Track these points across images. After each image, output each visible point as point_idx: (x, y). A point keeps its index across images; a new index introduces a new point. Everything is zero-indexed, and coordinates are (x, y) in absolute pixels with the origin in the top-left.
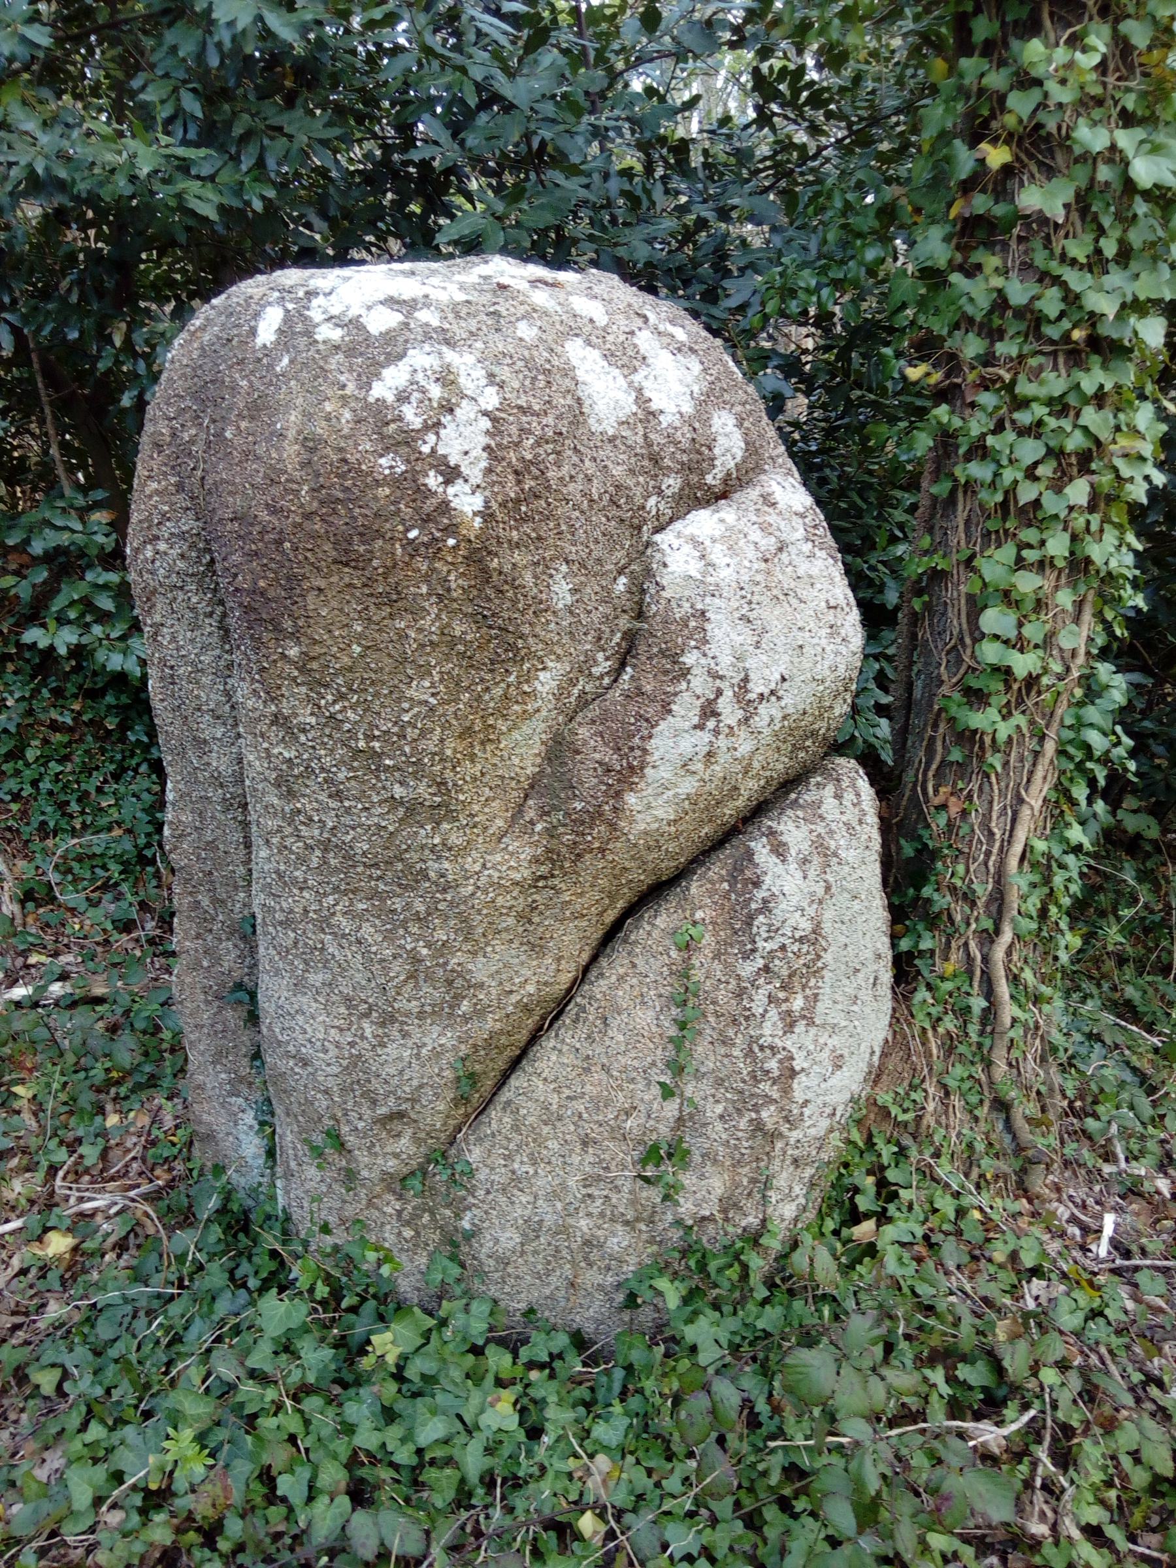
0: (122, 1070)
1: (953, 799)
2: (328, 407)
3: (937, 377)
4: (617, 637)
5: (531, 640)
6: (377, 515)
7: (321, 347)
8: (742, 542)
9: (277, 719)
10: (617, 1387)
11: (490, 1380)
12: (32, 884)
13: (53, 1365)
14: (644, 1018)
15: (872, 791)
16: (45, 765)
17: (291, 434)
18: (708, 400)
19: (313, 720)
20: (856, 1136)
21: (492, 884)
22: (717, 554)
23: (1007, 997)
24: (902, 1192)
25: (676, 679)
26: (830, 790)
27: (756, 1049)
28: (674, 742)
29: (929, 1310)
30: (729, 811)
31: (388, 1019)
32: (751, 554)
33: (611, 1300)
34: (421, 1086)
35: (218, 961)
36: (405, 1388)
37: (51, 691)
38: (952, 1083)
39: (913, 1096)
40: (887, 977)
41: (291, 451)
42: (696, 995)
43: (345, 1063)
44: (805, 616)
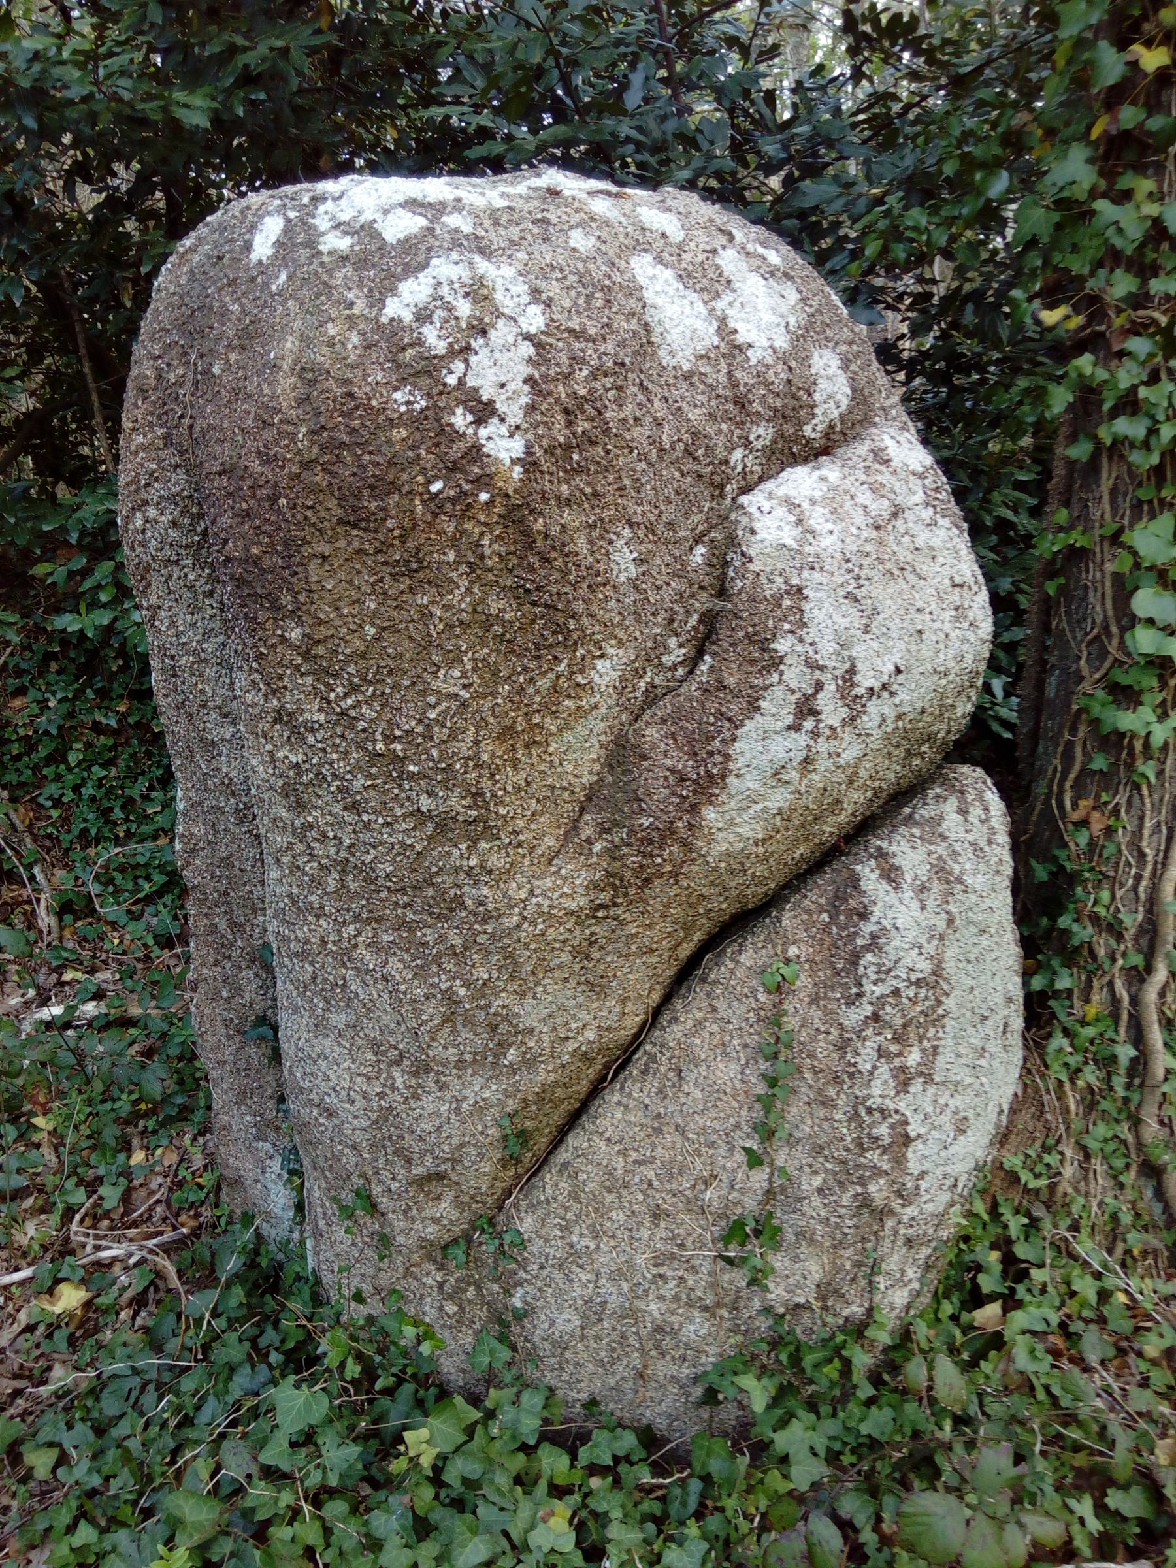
0: (152, 1101)
1: (1096, 815)
2: (331, 330)
3: (1078, 321)
4: (694, 619)
6: (391, 463)
7: (326, 259)
8: (848, 505)
9: (280, 716)
10: (692, 1505)
11: (543, 1486)
12: (70, 895)
13: (51, 1445)
14: (727, 1072)
15: (1001, 805)
17: (286, 365)
18: (807, 335)
19: (322, 718)
22: (818, 519)
23: (1159, 1045)
25: (765, 670)
26: (952, 804)
27: (863, 1113)
28: (763, 746)
29: (1070, 1419)
30: (829, 829)
31: (421, 1068)
32: (859, 518)
33: (688, 1394)
34: (462, 1145)
35: (237, 991)
36: (443, 1493)
37: (96, 692)
38: (1093, 1145)
41: (286, 384)
42: (789, 1047)
43: (374, 1116)
44: (924, 595)
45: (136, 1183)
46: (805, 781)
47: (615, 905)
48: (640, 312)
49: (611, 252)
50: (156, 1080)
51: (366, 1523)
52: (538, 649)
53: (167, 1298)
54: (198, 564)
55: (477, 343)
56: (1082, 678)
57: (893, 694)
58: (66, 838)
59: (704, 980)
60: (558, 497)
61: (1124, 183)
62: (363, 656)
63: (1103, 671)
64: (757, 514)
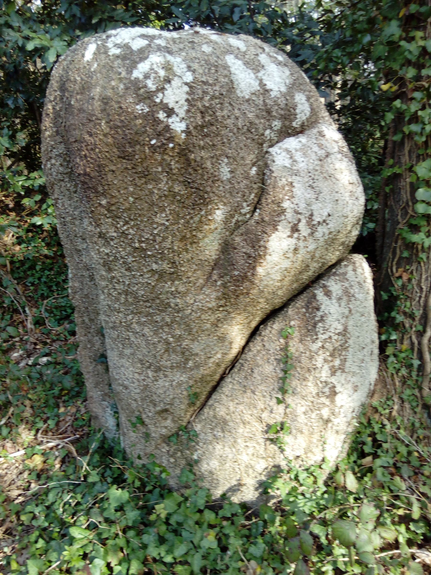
1: (405, 274)
3: (395, 88)
5: (211, 195)
6: (136, 133)
7: (111, 58)
8: (309, 152)
9: (101, 235)
11: (205, 526)
16: (43, 272)
17: (96, 98)
18: (294, 87)
19: (115, 234)
21: (199, 309)
22: (298, 156)
25: (279, 215)
26: (350, 268)
27: (319, 382)
29: (397, 497)
30: (306, 277)
31: (158, 369)
32: (314, 157)
34: (174, 398)
35: (93, 345)
36: (170, 527)
38: (405, 397)
39: (388, 403)
40: (376, 351)
41: (97, 104)
43: (141, 388)
45: (61, 419)
47: (226, 306)
48: (229, 75)
49: (218, 53)
50: (68, 382)
51: (141, 539)
54: (71, 180)
55: (167, 86)
57: (327, 224)
60: (199, 146)
61: (411, 34)
63: (406, 220)
64: (275, 155)
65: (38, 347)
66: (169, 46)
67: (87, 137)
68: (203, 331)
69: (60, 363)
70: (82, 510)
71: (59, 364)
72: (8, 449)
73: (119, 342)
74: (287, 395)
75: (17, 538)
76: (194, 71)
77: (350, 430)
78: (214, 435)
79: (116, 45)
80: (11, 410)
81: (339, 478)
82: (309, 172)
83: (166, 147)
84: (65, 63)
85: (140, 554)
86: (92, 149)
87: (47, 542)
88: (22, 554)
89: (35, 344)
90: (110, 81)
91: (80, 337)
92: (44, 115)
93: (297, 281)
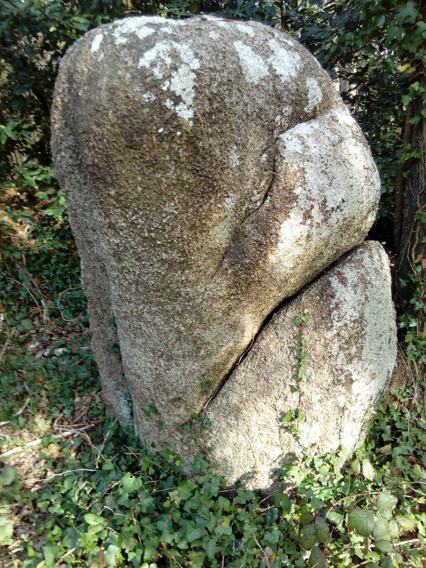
3: (413, 70)
6: (144, 122)
7: (118, 47)
8: (322, 137)
9: (111, 226)
16: (58, 265)
18: (305, 71)
19: (124, 225)
20: (382, 409)
22: (310, 142)
24: (403, 433)
25: (290, 202)
26: (367, 254)
27: (334, 370)
29: (417, 486)
30: (319, 264)
31: (170, 358)
32: (326, 142)
34: (187, 387)
35: (106, 335)
40: (395, 339)
41: (104, 94)
43: (154, 377)
45: (77, 408)
46: (308, 245)
47: (237, 294)
49: (226, 40)
50: (83, 373)
51: (155, 526)
52: (203, 194)
53: (87, 448)
54: (81, 172)
55: (174, 74)
56: (418, 208)
57: (341, 210)
58: (51, 289)
59: (273, 323)
60: (207, 133)
62: (138, 199)
64: (286, 141)
65: (54, 338)
66: (175, 33)
67: (94, 128)
68: (215, 320)
69: (75, 354)
70: (97, 498)
71: (74, 355)
72: (25, 438)
73: (130, 332)
74: (301, 383)
75: (34, 525)
76: (201, 58)
77: (367, 417)
78: (228, 424)
79: (123, 35)
80: (28, 400)
81: (356, 466)
82: (322, 158)
83: (174, 135)
84: (72, 55)
85: (155, 540)
86: (100, 140)
87: (63, 529)
88: (39, 541)
89: (51, 336)
90: (116, 71)
91: (93, 328)
92: (53, 108)
93: (310, 269)
